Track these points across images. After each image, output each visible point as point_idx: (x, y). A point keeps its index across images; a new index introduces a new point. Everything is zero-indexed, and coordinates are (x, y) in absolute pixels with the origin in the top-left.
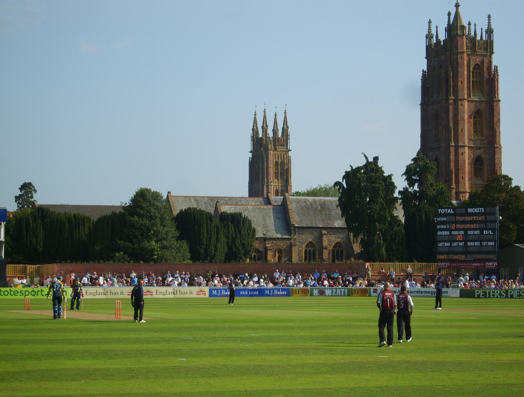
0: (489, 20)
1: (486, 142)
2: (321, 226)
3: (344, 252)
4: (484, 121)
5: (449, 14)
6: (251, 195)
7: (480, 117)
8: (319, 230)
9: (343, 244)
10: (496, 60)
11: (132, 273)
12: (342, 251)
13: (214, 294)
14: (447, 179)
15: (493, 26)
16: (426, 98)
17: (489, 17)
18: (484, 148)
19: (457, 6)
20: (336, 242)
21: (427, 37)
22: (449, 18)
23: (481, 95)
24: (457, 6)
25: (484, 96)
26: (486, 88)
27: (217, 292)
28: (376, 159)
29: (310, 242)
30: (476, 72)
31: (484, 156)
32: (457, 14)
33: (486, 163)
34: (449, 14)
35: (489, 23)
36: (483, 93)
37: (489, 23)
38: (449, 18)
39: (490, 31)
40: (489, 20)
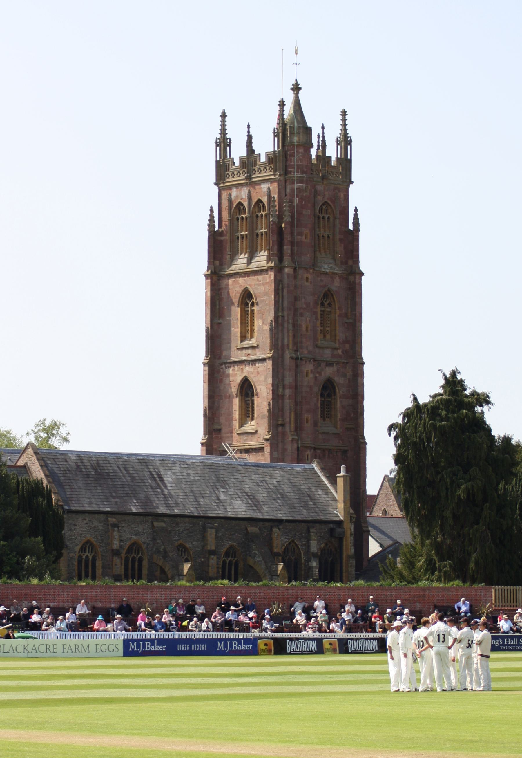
0: (344, 120)
1: (340, 352)
2: (108, 509)
3: (145, 563)
4: (338, 312)
5: (282, 104)
6: (207, 454)
7: (329, 304)
8: (102, 517)
9: (144, 547)
10: (358, 197)
11: (251, 611)
12: (140, 560)
13: (133, 650)
14: (280, 422)
15: (350, 133)
16: (217, 263)
17: (344, 113)
18: (338, 363)
19: (296, 88)
20: (132, 541)
21: (217, 144)
22: (282, 111)
23: (332, 261)
24: (296, 88)
25: (336, 264)
26: (340, 249)
27: (138, 646)
28: (430, 396)
29: (88, 542)
30: (323, 218)
31: (339, 380)
32: (297, 104)
33: (340, 392)
34: (282, 104)
35: (344, 125)
36: (334, 259)
37: (344, 125)
38: (282, 111)
39: (345, 141)
40: (344, 120)
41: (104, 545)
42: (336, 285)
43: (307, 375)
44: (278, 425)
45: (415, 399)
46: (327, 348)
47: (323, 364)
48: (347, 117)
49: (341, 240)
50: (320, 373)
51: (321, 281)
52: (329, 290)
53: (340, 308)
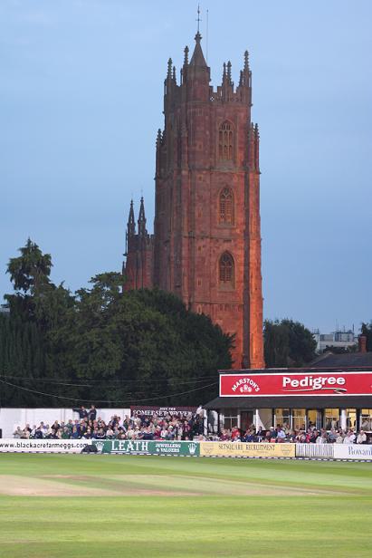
0: (246, 59)
4: (236, 202)
5: (187, 50)
19: (198, 38)
22: (186, 55)
24: (198, 38)
34: (187, 50)
35: (246, 62)
37: (246, 62)
40: (246, 59)
41: (172, 382)
42: (236, 181)
43: (200, 249)
44: (179, 286)
45: (29, 242)
46: (225, 228)
47: (221, 241)
48: (249, 57)
49: (240, 148)
50: (218, 248)
51: (220, 179)
52: (227, 186)
53: (239, 199)
